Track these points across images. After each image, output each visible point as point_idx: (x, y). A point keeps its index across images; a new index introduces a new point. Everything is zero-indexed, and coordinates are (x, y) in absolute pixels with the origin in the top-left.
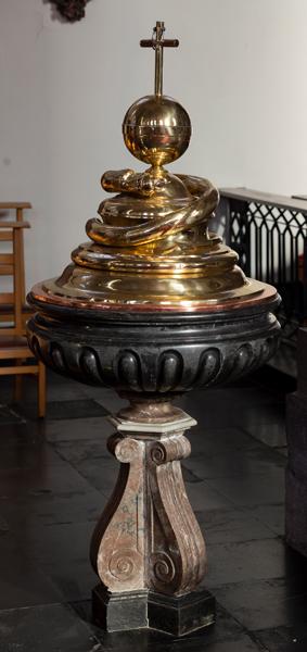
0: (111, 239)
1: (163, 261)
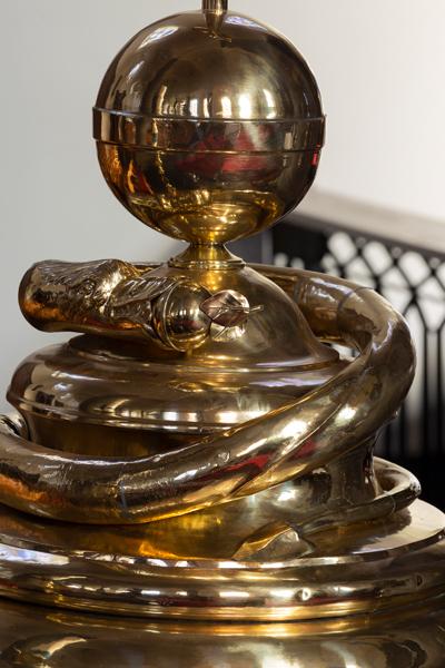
0: (52, 494)
1: (234, 579)
